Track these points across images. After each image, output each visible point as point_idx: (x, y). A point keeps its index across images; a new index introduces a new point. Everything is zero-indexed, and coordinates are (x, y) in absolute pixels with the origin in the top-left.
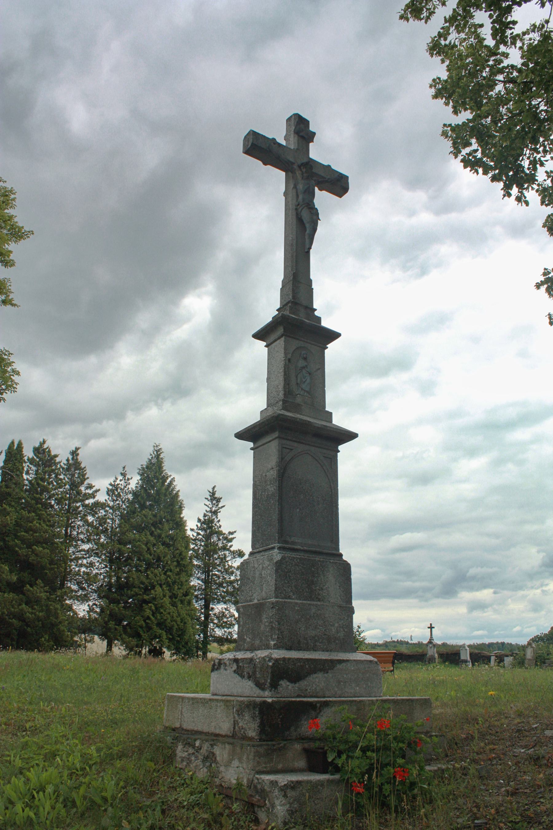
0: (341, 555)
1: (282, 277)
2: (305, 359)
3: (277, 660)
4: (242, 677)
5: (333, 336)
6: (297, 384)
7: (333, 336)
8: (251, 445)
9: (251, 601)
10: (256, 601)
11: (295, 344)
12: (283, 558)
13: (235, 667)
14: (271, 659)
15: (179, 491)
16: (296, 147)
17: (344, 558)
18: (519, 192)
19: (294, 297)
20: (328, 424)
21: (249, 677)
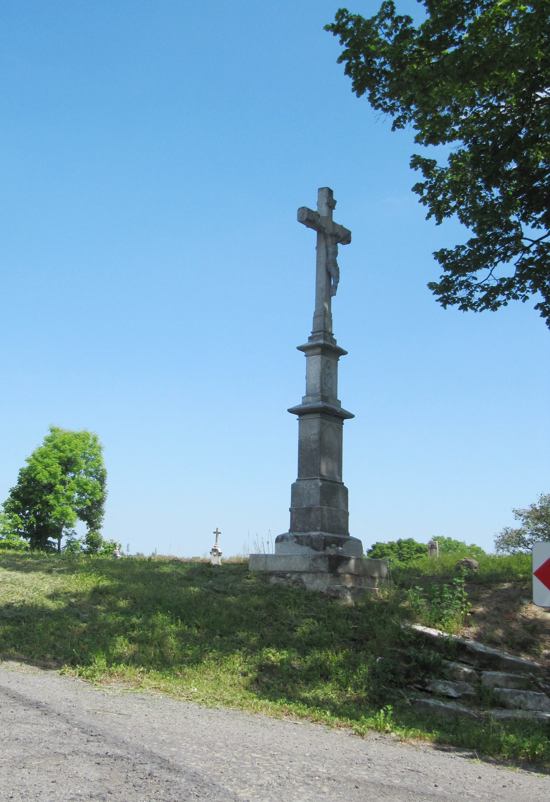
0: (343, 483)
1: (314, 310)
2: (329, 368)
3: (325, 536)
4: (302, 545)
5: (343, 353)
6: (325, 383)
7: (343, 353)
8: (297, 417)
9: (300, 506)
10: (304, 506)
11: (326, 358)
12: (323, 485)
13: (295, 540)
14: (323, 536)
15: (519, 514)
16: (327, 216)
17: (345, 485)
18: (461, 289)
19: (324, 328)
20: (336, 408)
21: (307, 545)
